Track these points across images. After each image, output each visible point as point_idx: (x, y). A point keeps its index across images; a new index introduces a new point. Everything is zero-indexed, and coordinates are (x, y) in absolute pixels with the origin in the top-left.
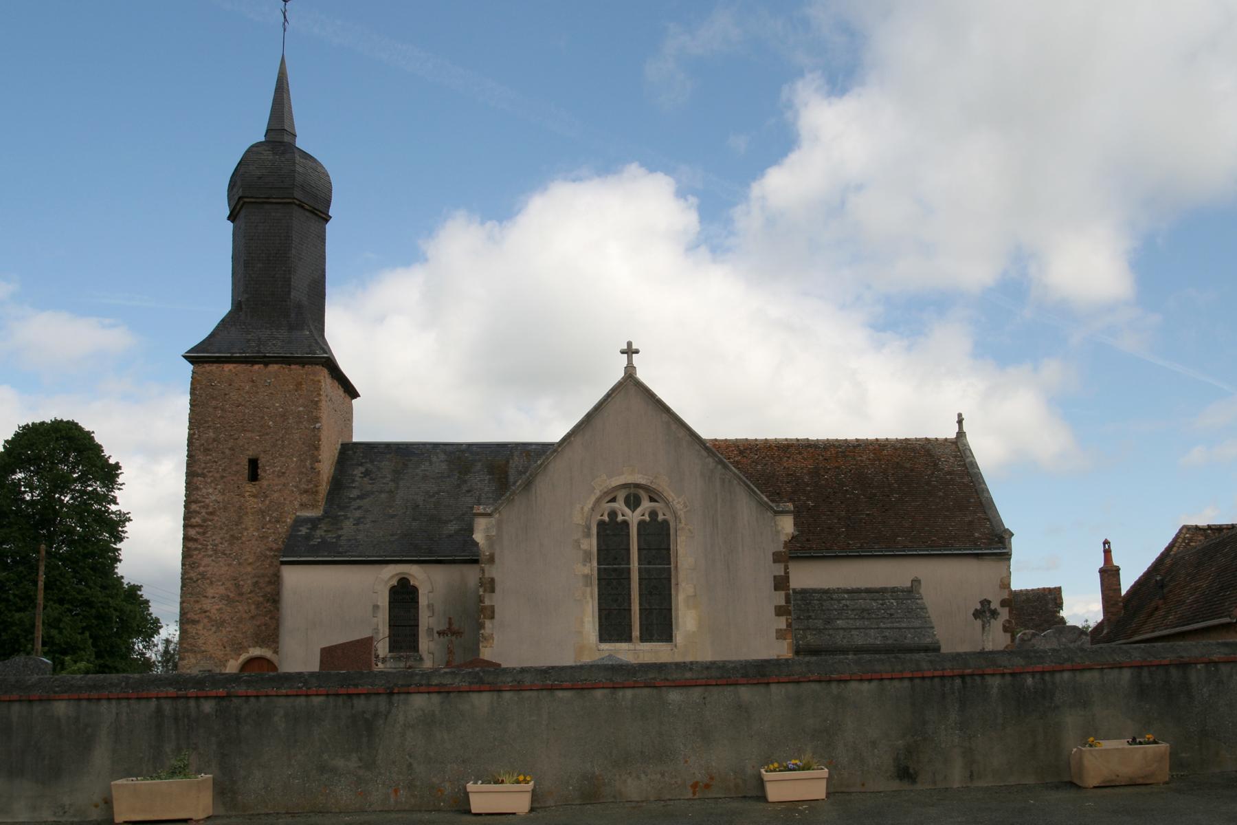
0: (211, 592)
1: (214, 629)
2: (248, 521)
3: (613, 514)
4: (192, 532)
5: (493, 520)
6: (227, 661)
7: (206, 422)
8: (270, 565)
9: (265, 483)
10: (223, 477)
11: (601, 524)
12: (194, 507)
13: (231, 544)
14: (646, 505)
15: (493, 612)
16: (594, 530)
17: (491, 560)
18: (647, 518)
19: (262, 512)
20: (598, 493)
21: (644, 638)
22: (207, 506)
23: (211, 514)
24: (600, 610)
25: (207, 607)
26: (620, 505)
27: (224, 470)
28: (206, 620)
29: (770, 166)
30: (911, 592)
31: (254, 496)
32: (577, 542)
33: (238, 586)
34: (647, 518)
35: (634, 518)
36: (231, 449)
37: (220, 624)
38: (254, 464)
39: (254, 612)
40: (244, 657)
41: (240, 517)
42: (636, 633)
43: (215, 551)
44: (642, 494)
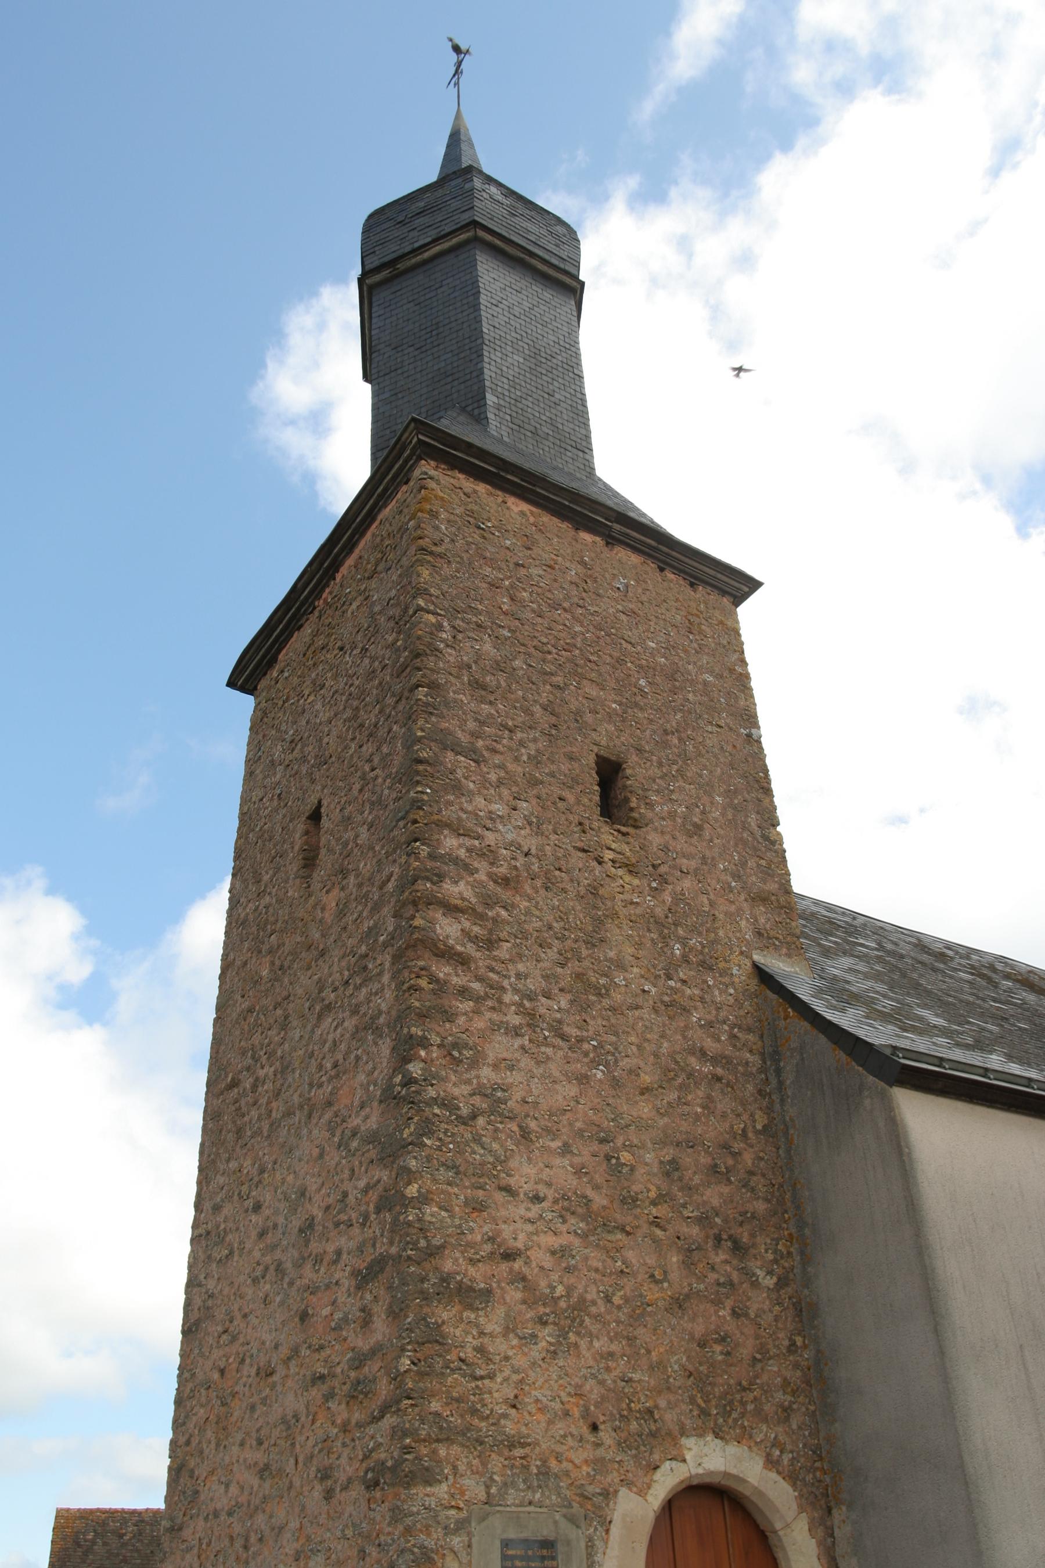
0: (525, 1173)
1: (547, 1335)
2: (620, 941)
6: (608, 1494)
8: (708, 1105)
10: (534, 782)
22: (489, 854)
23: (505, 882)
25: (514, 1234)
28: (514, 1295)
29: (69, 899)
30: (642, 1492)
33: (615, 1168)
37: (568, 1318)
38: (609, 772)
39: (678, 1279)
40: (666, 1481)
43: (532, 1018)
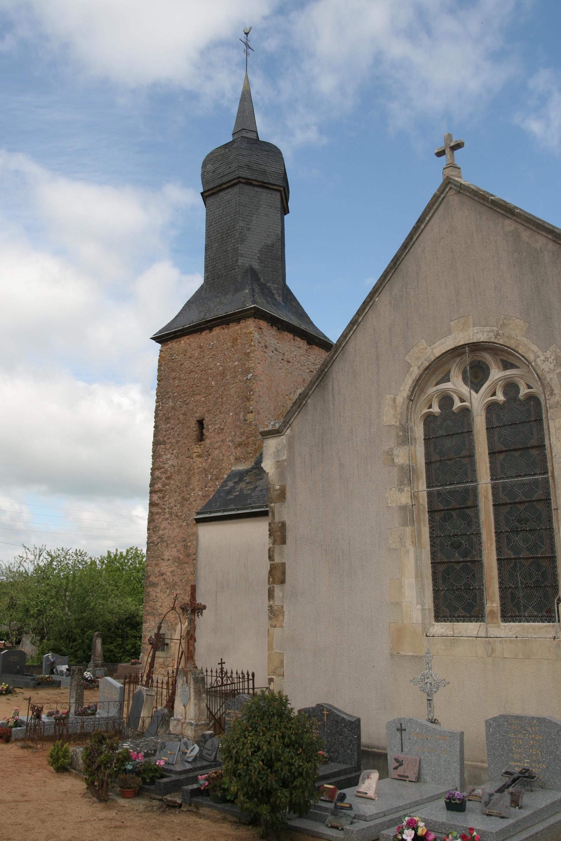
0: (167, 555)
1: (168, 591)
2: (195, 482)
3: (446, 400)
4: (155, 497)
5: (283, 439)
7: (168, 393)
9: (208, 441)
11: (429, 419)
12: (157, 473)
13: (182, 506)
14: (496, 374)
15: (284, 573)
16: (419, 431)
17: (282, 496)
18: (500, 397)
19: (205, 470)
20: (415, 372)
21: (507, 615)
24: (434, 564)
25: (163, 569)
26: (457, 385)
27: (179, 435)
31: (199, 456)
32: (390, 454)
34: (500, 397)
35: (478, 401)
36: (185, 414)
41: (189, 479)
42: (493, 603)
44: (488, 358)
